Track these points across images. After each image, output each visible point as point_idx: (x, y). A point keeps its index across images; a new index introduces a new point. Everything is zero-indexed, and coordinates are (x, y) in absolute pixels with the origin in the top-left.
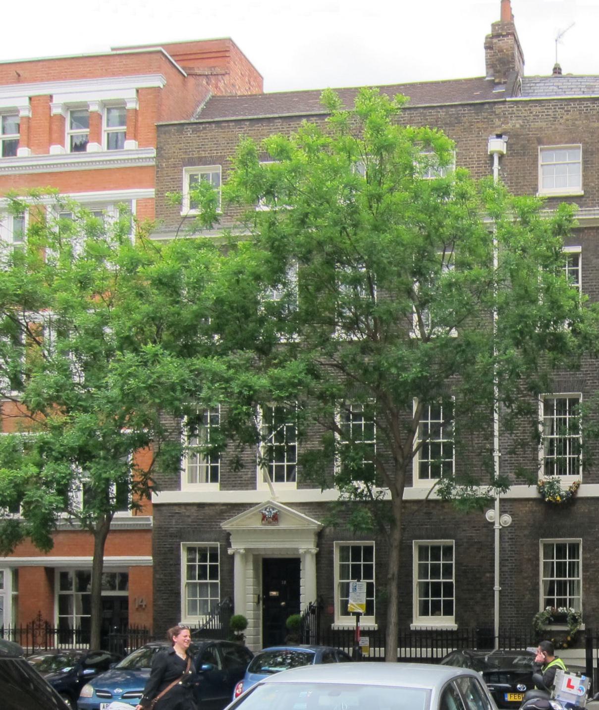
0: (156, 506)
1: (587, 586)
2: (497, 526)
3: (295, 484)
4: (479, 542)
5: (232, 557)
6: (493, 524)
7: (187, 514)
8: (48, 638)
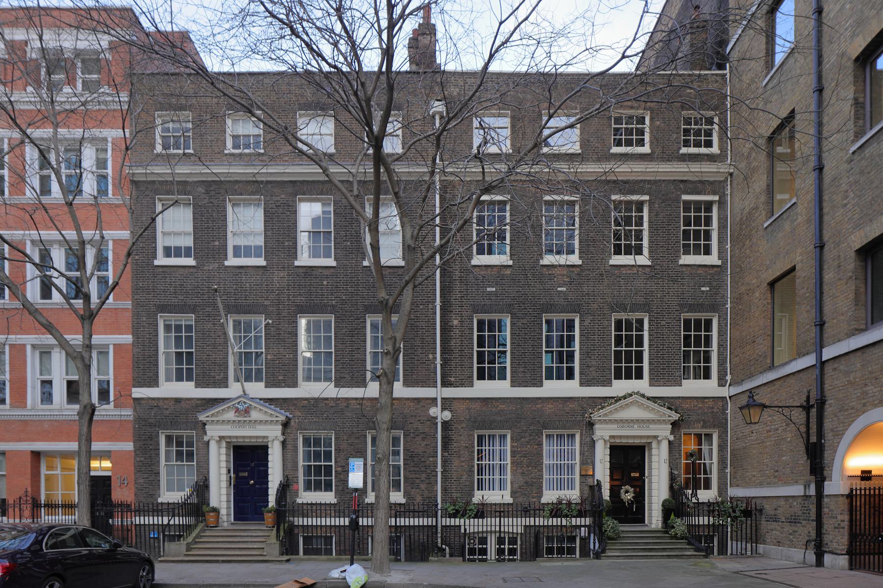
0: (135, 399)
1: (515, 468)
2: (439, 420)
3: (193, 384)
4: (424, 433)
5: (208, 443)
6: (436, 418)
7: (165, 407)
8: (35, 511)
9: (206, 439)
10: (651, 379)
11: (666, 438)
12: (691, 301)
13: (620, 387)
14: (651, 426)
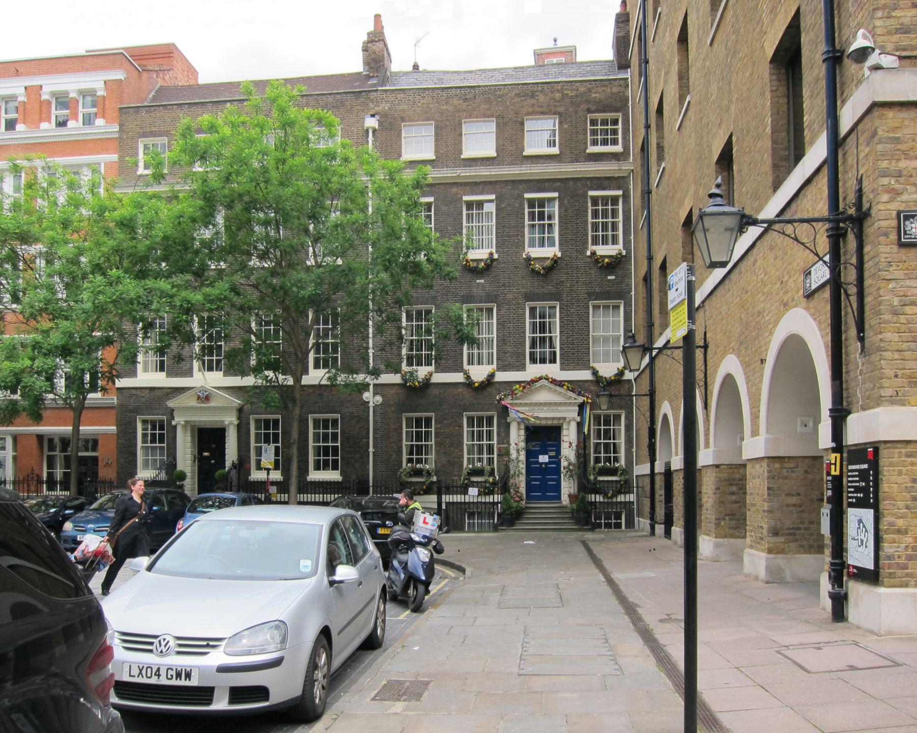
0: (119, 389)
2: (371, 404)
5: (175, 427)
6: (368, 402)
9: (174, 423)
10: (562, 364)
11: (574, 419)
12: (597, 289)
13: (533, 371)
14: (559, 408)
